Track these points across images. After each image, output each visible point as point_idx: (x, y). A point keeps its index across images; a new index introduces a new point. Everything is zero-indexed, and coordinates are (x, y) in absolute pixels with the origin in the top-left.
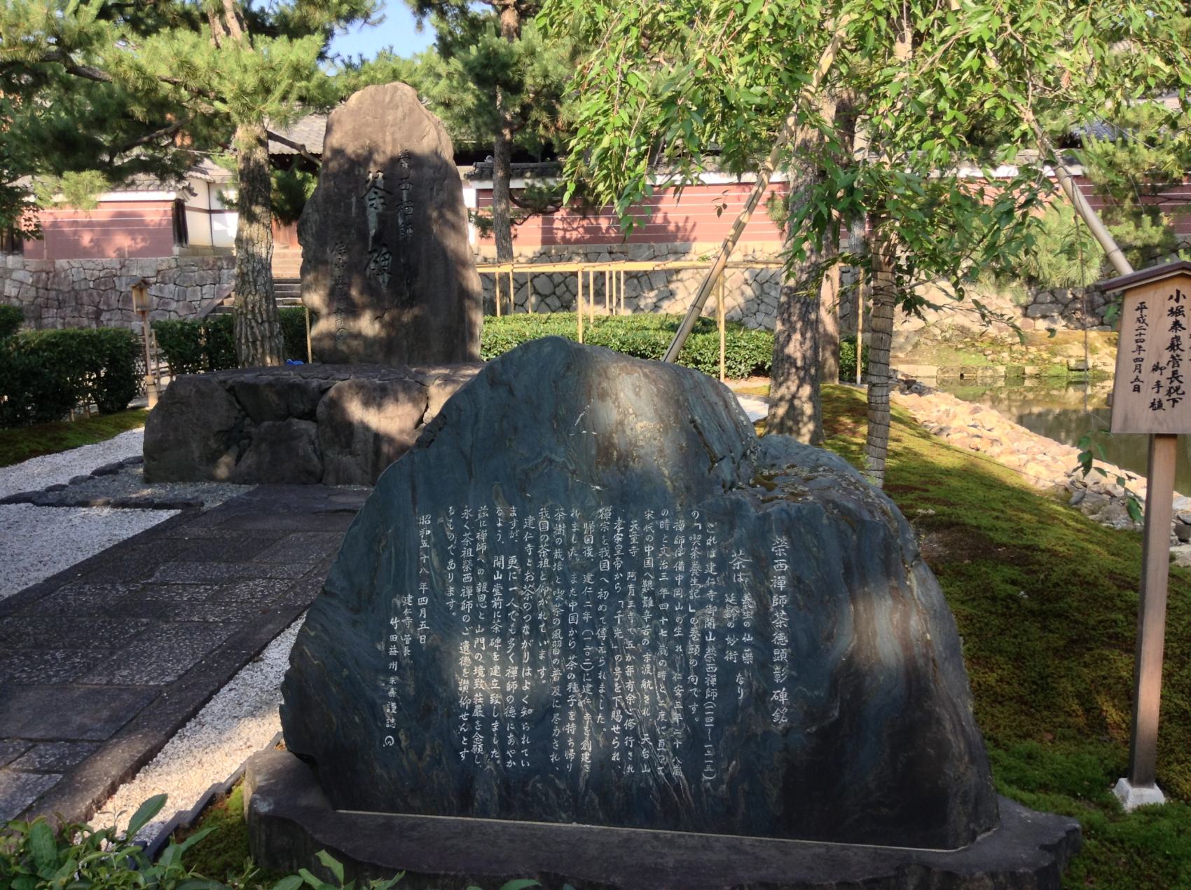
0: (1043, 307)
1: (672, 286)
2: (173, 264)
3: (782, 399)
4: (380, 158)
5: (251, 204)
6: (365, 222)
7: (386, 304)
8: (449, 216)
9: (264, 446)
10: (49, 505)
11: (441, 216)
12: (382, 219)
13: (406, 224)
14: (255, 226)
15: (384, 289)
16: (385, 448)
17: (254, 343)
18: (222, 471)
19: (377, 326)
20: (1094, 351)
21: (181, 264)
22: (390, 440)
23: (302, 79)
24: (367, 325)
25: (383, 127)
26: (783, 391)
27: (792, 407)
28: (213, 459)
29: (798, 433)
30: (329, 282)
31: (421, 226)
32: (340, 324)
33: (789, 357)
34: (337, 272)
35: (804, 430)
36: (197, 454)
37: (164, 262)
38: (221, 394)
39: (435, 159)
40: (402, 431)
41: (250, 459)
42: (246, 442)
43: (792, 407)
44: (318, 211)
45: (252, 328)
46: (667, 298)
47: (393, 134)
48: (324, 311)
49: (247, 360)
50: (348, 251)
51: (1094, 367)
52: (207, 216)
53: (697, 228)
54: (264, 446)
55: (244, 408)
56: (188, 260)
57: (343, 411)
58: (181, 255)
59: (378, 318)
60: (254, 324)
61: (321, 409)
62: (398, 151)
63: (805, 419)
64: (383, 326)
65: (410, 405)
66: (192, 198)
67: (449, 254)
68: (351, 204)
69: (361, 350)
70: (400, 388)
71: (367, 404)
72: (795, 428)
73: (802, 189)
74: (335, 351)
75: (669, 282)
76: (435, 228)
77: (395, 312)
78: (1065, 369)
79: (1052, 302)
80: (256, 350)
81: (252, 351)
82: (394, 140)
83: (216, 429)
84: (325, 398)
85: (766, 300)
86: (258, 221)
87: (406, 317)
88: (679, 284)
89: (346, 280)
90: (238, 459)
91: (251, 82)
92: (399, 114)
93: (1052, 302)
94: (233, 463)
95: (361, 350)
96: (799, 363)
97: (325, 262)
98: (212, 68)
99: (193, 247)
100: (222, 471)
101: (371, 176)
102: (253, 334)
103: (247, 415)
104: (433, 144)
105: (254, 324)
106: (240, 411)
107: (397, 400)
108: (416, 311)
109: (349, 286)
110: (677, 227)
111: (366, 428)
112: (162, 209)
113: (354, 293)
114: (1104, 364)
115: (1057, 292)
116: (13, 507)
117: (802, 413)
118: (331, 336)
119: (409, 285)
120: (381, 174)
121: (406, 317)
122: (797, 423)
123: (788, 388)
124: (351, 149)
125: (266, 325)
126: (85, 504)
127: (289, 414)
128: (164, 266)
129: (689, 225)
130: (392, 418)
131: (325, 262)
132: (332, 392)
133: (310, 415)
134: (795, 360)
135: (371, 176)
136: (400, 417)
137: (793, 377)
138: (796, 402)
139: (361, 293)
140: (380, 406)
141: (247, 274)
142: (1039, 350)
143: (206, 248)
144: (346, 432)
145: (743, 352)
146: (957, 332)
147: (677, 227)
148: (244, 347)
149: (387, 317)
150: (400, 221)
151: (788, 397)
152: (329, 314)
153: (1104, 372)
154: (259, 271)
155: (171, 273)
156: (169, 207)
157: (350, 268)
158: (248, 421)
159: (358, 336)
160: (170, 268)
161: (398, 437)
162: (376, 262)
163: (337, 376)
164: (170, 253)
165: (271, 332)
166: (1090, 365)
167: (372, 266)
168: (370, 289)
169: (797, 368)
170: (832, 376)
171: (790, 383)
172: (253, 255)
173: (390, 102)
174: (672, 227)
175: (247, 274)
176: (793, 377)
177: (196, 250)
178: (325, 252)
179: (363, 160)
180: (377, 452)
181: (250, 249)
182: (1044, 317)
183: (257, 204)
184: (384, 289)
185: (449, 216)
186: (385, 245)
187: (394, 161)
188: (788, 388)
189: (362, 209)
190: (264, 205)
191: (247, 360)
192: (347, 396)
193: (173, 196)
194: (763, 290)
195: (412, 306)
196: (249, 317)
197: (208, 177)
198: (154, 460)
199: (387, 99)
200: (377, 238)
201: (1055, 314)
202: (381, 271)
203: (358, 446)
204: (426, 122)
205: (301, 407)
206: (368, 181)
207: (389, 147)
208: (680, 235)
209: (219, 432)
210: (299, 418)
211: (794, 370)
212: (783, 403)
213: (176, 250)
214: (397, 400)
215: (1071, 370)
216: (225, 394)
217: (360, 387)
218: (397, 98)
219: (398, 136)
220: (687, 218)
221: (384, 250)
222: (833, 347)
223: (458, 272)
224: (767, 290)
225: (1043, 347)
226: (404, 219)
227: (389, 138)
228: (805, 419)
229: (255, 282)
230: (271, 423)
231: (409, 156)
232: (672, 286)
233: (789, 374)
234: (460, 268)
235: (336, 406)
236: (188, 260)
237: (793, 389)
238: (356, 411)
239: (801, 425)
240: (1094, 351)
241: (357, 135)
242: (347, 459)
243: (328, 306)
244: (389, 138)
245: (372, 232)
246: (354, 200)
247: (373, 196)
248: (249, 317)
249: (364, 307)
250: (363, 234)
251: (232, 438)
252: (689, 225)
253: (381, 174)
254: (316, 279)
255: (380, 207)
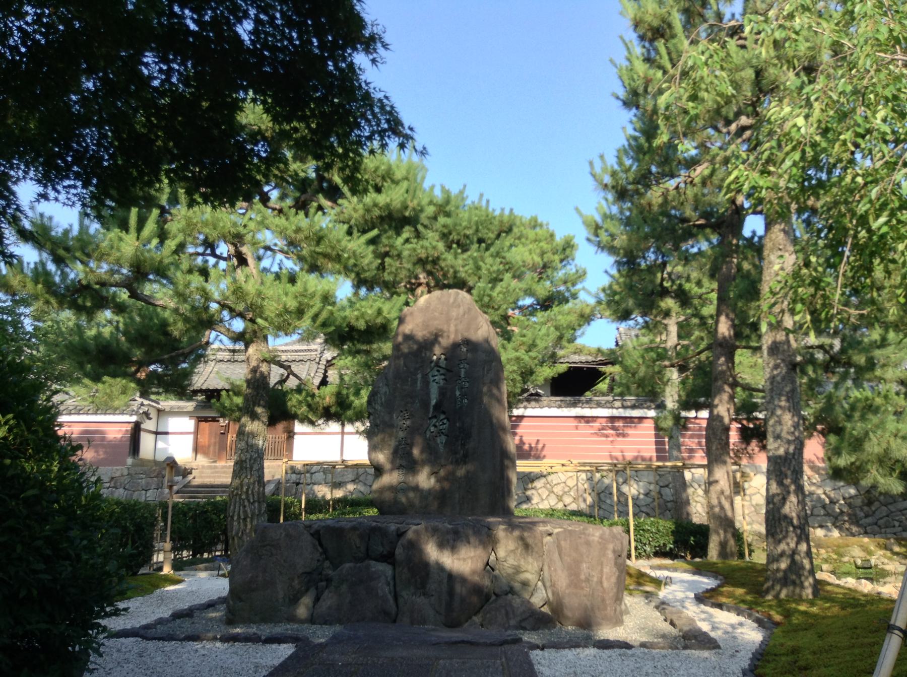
0: (819, 518)
1: (529, 493)
2: (126, 472)
3: (782, 554)
4: (445, 342)
5: (254, 406)
6: (428, 394)
7: (443, 461)
8: (495, 391)
9: (344, 588)
10: (159, 639)
11: (490, 391)
12: (442, 392)
13: (463, 396)
14: (256, 423)
15: (441, 448)
16: (458, 588)
17: (245, 519)
18: (302, 611)
19: (433, 480)
20: (870, 553)
21: (132, 472)
22: (463, 580)
23: (329, 304)
24: (425, 479)
25: (448, 320)
26: (782, 546)
27: (793, 562)
28: (294, 600)
29: (802, 587)
30: (393, 443)
31: (474, 397)
32: (402, 478)
33: (786, 517)
34: (401, 434)
35: (806, 584)
36: (281, 595)
37: (118, 470)
38: (307, 538)
39: (487, 345)
40: (474, 572)
41: (329, 600)
42: (324, 584)
43: (793, 562)
44: (387, 385)
45: (245, 507)
46: (524, 502)
47: (456, 326)
48: (388, 466)
49: (237, 534)
50: (411, 416)
51: (876, 566)
52: (153, 436)
53: (546, 448)
54: (344, 588)
55: (325, 552)
56: (139, 469)
57: (421, 552)
58: (133, 465)
59: (433, 473)
60: (246, 503)
61: (399, 551)
62: (459, 338)
63: (806, 573)
64: (438, 481)
65: (481, 547)
66: (148, 421)
67: (495, 421)
68: (417, 379)
69: (417, 502)
70: (470, 532)
71: (441, 546)
72: (798, 582)
73: (779, 379)
74: (396, 502)
75: (526, 489)
76: (485, 400)
77: (450, 467)
78: (854, 567)
79: (825, 515)
80: (246, 526)
81: (242, 526)
82: (456, 331)
83: (301, 571)
84: (403, 541)
85: (603, 506)
86: (259, 419)
87: (461, 472)
88: (533, 491)
89: (409, 441)
90: (317, 599)
91: (292, 304)
92: (461, 311)
93: (825, 515)
94: (311, 605)
95: (417, 502)
96: (795, 521)
97: (392, 426)
98: (259, 294)
99: (141, 460)
100: (302, 611)
101: (435, 357)
102: (245, 512)
103: (327, 559)
104: (485, 335)
105: (246, 503)
106: (321, 554)
107: (469, 543)
108: (470, 467)
109: (411, 446)
110: (531, 447)
111: (440, 568)
112: (124, 429)
113: (416, 452)
114: (883, 563)
115: (827, 507)
116: (122, 640)
117: (803, 568)
118: (392, 488)
119: (463, 445)
120: (443, 357)
121: (461, 472)
122: (799, 576)
123: (788, 544)
124: (420, 334)
125: (256, 504)
126: (194, 638)
127: (368, 556)
128: (118, 474)
129: (540, 446)
130: (464, 560)
131: (392, 426)
132: (410, 535)
133: (388, 558)
134: (792, 519)
135: (435, 357)
136: (472, 558)
137: (791, 534)
138: (797, 557)
139: (422, 452)
140: (453, 549)
141: (245, 461)
142: (827, 552)
143: (149, 461)
144: (422, 573)
145: (647, 535)
146: (756, 538)
147: (531, 447)
148: (235, 523)
149: (442, 473)
150: (458, 393)
151: (788, 552)
152: (392, 470)
153: (883, 570)
154: (255, 460)
155: (122, 479)
156: (129, 427)
157: (413, 431)
158: (327, 564)
159: (416, 489)
160: (122, 476)
161: (470, 578)
162: (435, 426)
163: (410, 521)
164: (124, 464)
165: (260, 511)
166: (873, 564)
167: (432, 429)
168: (430, 449)
169: (794, 527)
170: (732, 555)
171: (789, 540)
172: (252, 446)
173: (454, 302)
174: (526, 447)
175: (245, 461)
176: (791, 534)
177: (144, 462)
178: (392, 418)
179: (428, 344)
180: (451, 593)
181: (250, 440)
182: (821, 526)
183: (259, 405)
184: (441, 448)
185: (495, 391)
186: (444, 413)
187: (456, 346)
188: (788, 544)
189: (426, 383)
190: (264, 407)
191: (237, 534)
192: (424, 537)
193: (134, 418)
194: (600, 498)
195: (465, 463)
196: (243, 497)
197: (159, 406)
198: (241, 600)
199: (452, 300)
200: (437, 407)
201: (829, 524)
202: (440, 433)
203: (432, 586)
204: (480, 319)
205: (381, 549)
206: (432, 362)
207: (452, 334)
208: (533, 453)
209: (303, 573)
210: (376, 560)
211: (791, 529)
212: (784, 559)
213: (130, 461)
214: (469, 543)
215: (858, 567)
216: (310, 538)
217: (435, 531)
218: (459, 300)
219: (460, 327)
220: (538, 441)
221: (442, 417)
222: (732, 530)
223: (499, 437)
224: (603, 499)
225: (829, 550)
226: (461, 391)
227: (452, 328)
228: (806, 573)
229: (251, 468)
230: (351, 565)
231: (467, 342)
232: (529, 493)
233: (787, 532)
234: (501, 433)
235: (414, 547)
236: (139, 469)
237: (793, 545)
238: (432, 552)
239: (803, 578)
240: (870, 553)
241: (426, 325)
242: (420, 600)
243: (392, 462)
244: (452, 328)
245: (433, 402)
246: (419, 376)
247: (436, 373)
248: (243, 497)
249: (424, 463)
250: (425, 404)
251: (315, 581)
252: (540, 446)
253: (443, 357)
254: (383, 440)
255: (442, 382)
